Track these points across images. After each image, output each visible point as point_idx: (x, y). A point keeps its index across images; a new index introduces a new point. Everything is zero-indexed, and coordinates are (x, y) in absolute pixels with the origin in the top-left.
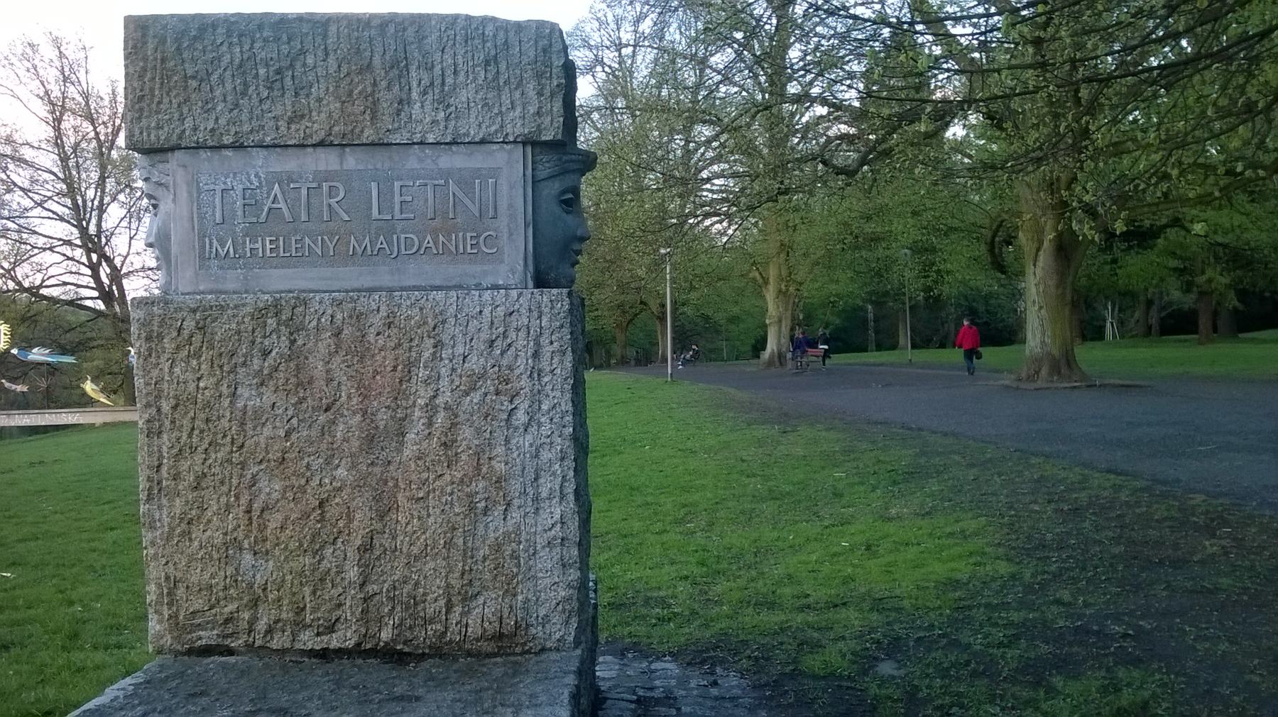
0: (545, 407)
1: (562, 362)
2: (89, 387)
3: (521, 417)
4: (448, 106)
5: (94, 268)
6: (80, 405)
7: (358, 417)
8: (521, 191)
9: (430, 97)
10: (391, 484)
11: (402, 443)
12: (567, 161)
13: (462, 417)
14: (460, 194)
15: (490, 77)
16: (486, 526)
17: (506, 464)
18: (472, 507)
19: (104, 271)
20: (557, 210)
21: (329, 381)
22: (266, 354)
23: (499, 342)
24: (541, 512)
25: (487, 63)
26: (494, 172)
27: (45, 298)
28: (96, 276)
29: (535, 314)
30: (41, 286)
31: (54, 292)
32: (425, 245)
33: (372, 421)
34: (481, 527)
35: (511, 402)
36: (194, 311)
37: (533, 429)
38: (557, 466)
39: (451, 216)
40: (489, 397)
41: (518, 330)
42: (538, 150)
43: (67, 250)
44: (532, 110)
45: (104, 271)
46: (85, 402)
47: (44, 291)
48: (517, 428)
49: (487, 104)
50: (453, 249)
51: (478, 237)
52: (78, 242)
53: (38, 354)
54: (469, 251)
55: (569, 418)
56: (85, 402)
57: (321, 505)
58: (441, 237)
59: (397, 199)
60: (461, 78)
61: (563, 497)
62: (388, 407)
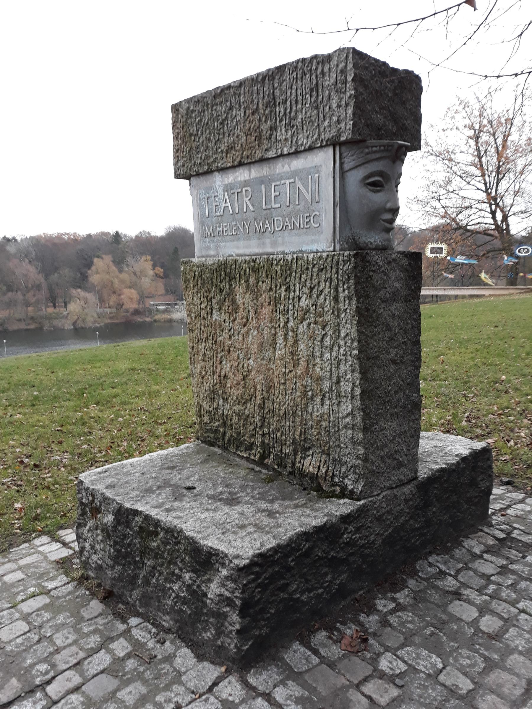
0: (342, 335)
1: (350, 304)
2: (483, 276)
3: (328, 341)
4: (293, 126)
5: (493, 213)
6: (480, 285)
7: (256, 332)
8: (331, 180)
9: (283, 123)
10: (271, 372)
11: (275, 349)
12: (368, 154)
13: (300, 337)
14: (301, 188)
15: (313, 100)
16: (313, 407)
17: (322, 370)
18: (304, 394)
19: (499, 216)
20: (366, 192)
21: (245, 309)
22: (221, 291)
23: (315, 290)
24: (342, 404)
25: (312, 90)
26: (317, 169)
27: (469, 231)
28: (494, 218)
29: (334, 270)
30: (467, 225)
31: (472, 228)
32: (286, 224)
33: (262, 334)
34: (310, 408)
35: (323, 329)
36: (198, 267)
37: (336, 349)
38: (350, 376)
39: (288, 204)
40: (312, 325)
41: (326, 281)
42: (343, 149)
43: (480, 206)
44: (335, 118)
45: (499, 216)
46: (481, 284)
47: (468, 228)
48: (326, 347)
49: (311, 121)
50: (298, 226)
51: (310, 216)
52: (487, 201)
53: (460, 259)
54: (306, 226)
55: (356, 344)
56: (481, 284)
57: (244, 379)
58: (293, 219)
59: (273, 194)
60: (299, 106)
61: (353, 397)
62: (268, 327)
